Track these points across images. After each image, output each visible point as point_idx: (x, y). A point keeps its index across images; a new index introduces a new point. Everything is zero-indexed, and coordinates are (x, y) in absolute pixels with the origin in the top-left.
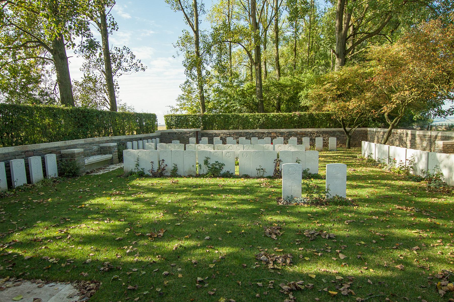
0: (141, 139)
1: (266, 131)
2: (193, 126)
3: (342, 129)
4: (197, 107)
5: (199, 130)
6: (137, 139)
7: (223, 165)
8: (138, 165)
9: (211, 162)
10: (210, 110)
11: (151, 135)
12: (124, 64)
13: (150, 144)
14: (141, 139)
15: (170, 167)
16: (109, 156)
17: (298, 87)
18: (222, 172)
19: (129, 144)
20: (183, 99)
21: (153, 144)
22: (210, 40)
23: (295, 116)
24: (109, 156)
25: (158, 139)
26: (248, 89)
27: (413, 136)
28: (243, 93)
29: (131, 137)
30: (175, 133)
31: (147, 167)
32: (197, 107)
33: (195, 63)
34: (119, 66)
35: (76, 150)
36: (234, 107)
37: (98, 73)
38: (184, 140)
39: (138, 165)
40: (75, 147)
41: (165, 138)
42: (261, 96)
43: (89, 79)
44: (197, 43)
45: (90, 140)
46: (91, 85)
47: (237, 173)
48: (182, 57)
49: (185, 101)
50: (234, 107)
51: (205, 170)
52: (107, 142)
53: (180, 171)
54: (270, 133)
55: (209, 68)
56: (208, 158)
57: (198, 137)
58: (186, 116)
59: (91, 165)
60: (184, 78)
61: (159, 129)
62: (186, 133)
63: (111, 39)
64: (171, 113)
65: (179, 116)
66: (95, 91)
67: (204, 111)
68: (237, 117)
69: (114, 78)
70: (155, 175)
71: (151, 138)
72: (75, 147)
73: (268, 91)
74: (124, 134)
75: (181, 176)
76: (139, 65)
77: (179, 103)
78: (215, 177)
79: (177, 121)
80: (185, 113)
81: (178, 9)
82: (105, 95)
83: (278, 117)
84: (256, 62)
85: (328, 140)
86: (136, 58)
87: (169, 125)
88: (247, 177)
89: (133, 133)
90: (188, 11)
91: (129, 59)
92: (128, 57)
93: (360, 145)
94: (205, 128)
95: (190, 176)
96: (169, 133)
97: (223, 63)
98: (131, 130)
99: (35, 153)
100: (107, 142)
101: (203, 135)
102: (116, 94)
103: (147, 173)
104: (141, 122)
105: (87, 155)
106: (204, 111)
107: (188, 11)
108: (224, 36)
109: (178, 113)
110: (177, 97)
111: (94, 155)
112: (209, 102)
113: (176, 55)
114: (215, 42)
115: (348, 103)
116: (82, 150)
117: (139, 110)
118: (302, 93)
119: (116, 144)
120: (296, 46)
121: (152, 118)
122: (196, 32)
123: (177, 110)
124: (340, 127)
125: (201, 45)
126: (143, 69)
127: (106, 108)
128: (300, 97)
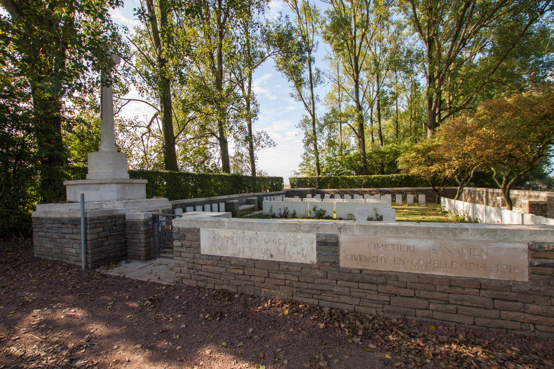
0: (272, 195)
1: (368, 189)
2: (310, 186)
3: (431, 188)
4: (314, 171)
5: (315, 188)
6: (270, 195)
7: (325, 211)
8: (271, 210)
9: (318, 209)
10: (324, 173)
11: (279, 192)
12: (262, 143)
13: (279, 198)
14: (272, 195)
15: (291, 212)
16: (252, 206)
17: (397, 154)
18: (324, 216)
19: (265, 198)
20: (304, 165)
21: (281, 198)
22: (322, 122)
23: (392, 177)
24: (252, 206)
25: (284, 196)
26: (354, 156)
27: (487, 192)
28: (351, 160)
29: (265, 193)
30: (297, 191)
31: (276, 211)
32: (314, 171)
33: (312, 139)
34: (258, 144)
35: (235, 201)
36: (342, 171)
37: (244, 150)
38: (302, 195)
39: (271, 210)
40: (233, 199)
41: (289, 194)
42: (365, 162)
43: (238, 154)
44: (314, 124)
45: (241, 195)
46: (239, 158)
47: (335, 217)
48: (303, 136)
49: (305, 167)
50: (342, 171)
51: (313, 214)
52: (251, 196)
53: (298, 214)
54: (371, 191)
55: (322, 142)
56: (315, 207)
57: (313, 194)
58: (305, 178)
59: (243, 210)
60: (304, 151)
61: (285, 188)
62: (304, 191)
63: (253, 125)
64: (294, 176)
65: (300, 178)
66: (242, 162)
67: (319, 174)
68: (345, 178)
69: (255, 152)
70: (282, 217)
71: (279, 194)
72: (233, 199)
73: (370, 157)
74: (261, 192)
75: (297, 218)
76: (272, 143)
77: (300, 168)
78: (320, 218)
79: (299, 182)
80: (305, 176)
81: (300, 100)
82: (248, 165)
83: (378, 178)
84: (361, 136)
85: (418, 197)
86: (270, 139)
87: (292, 185)
88: (341, 219)
89: (266, 191)
90: (307, 101)
91: (265, 139)
92: (264, 137)
93: (439, 202)
94: (319, 188)
95: (303, 218)
96: (292, 191)
97: (332, 139)
98: (265, 189)
99: (214, 202)
100: (251, 196)
101: (318, 193)
102: (256, 163)
103: (277, 215)
104: (272, 183)
105: (241, 204)
106: (319, 174)
107: (307, 101)
108: (335, 118)
109: (300, 176)
110: (299, 164)
111: (244, 205)
112: (323, 167)
113: (298, 134)
114: (327, 123)
115: (430, 167)
116: (238, 201)
117: (271, 175)
118: (400, 159)
119: (256, 198)
120: (397, 119)
121: (280, 180)
122: (313, 116)
123: (299, 174)
124: (430, 186)
125: (317, 126)
126: (274, 146)
127: (249, 174)
128: (397, 162)
